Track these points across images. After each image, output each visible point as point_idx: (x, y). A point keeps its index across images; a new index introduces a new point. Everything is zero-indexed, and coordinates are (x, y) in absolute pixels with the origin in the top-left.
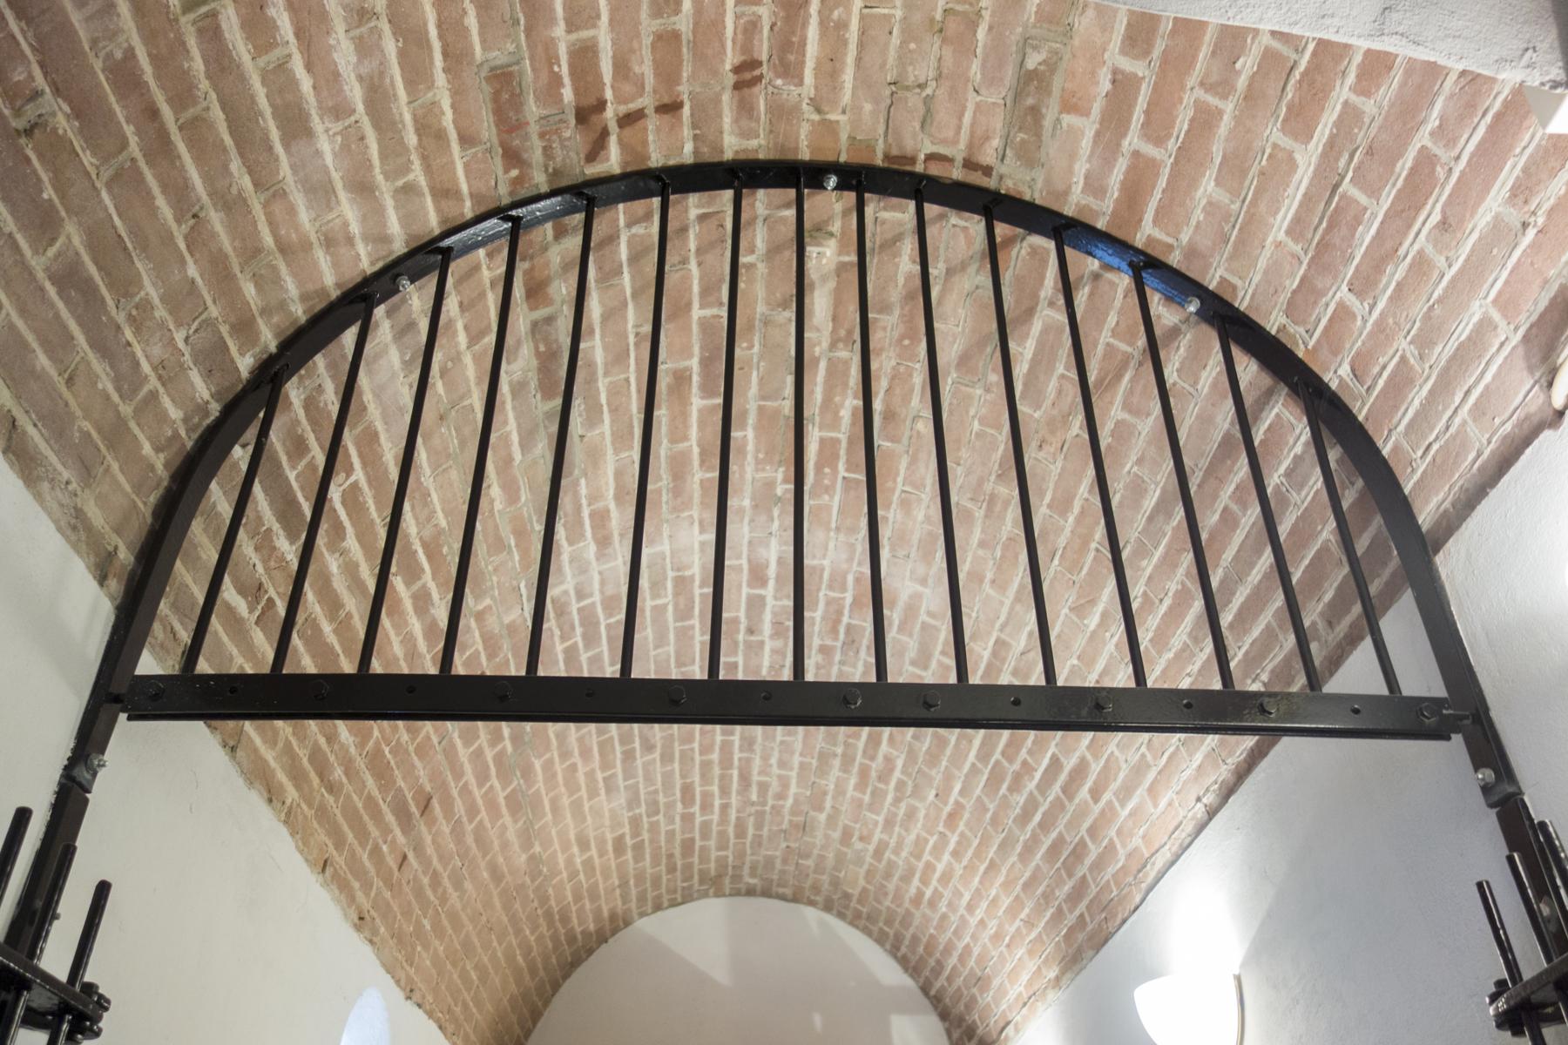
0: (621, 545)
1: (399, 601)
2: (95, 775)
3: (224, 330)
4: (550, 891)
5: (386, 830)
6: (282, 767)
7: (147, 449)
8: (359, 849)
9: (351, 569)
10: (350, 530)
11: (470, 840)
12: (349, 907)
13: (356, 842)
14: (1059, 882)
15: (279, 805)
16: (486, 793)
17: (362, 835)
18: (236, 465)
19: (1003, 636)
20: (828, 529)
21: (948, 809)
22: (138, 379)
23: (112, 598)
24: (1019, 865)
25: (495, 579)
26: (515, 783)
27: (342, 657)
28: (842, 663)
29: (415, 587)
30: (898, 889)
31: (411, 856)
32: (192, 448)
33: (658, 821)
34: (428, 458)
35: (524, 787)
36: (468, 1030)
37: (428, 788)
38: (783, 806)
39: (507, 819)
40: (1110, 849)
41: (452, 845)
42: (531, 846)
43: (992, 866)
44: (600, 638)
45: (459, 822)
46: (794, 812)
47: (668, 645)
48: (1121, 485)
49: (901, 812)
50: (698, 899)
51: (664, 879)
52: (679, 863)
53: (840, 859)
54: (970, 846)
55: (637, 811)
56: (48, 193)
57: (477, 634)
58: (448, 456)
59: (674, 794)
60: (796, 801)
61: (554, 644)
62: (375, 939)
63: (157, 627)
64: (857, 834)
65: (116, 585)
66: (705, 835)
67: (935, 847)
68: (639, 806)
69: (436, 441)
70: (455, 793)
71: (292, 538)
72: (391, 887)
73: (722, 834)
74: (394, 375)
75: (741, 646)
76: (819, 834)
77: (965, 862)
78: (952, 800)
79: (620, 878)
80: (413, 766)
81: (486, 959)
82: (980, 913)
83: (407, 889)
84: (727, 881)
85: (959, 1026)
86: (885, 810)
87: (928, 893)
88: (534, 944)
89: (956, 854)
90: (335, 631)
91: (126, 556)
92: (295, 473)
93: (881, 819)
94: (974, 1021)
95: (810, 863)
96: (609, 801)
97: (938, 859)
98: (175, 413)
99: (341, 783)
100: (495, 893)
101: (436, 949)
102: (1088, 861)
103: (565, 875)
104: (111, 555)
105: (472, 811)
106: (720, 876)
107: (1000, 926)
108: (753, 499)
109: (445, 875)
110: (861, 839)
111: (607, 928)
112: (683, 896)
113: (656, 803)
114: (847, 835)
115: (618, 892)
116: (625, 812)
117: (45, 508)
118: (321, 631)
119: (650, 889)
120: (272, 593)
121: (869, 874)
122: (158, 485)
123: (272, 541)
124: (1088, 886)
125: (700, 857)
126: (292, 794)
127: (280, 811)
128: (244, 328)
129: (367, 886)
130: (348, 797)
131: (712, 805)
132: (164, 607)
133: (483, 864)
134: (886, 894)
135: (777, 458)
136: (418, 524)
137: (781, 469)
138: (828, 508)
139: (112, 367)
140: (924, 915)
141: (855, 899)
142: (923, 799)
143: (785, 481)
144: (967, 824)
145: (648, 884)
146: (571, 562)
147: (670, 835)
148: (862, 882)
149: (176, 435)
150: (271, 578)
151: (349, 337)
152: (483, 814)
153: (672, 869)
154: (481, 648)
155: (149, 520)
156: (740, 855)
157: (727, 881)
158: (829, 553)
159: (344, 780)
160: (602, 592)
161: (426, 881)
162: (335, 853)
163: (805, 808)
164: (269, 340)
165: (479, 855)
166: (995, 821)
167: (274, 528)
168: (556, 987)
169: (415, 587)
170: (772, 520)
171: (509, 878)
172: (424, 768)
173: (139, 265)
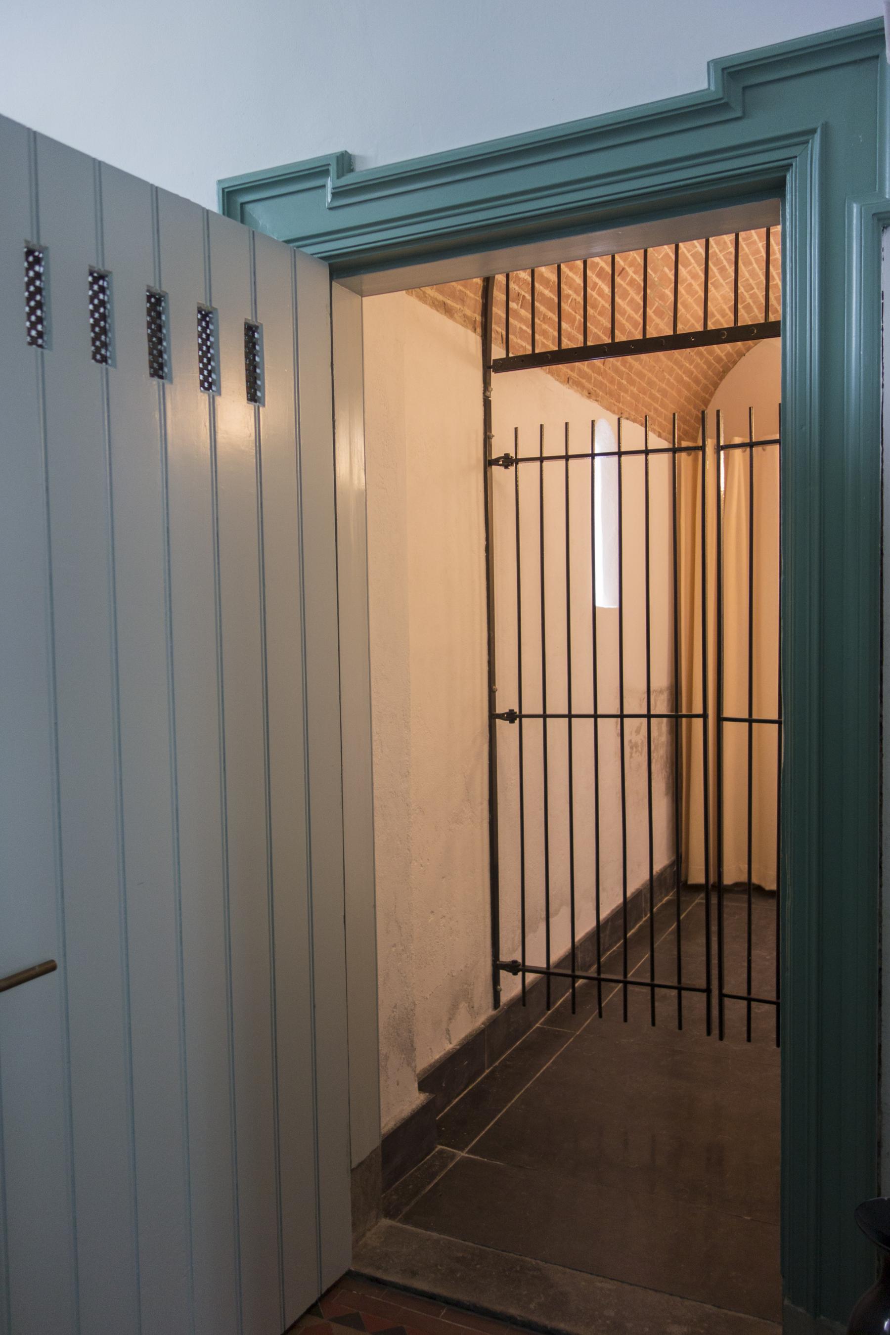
12: (583, 391)
18: (500, 282)
23: (478, 335)
26: (657, 304)
35: (662, 304)
36: (660, 420)
62: (598, 399)
63: (493, 335)
65: (479, 330)
80: (599, 321)
88: (694, 369)
91: (479, 318)
120: (523, 293)
132: (493, 326)
168: (716, 385)
172: (605, 319)
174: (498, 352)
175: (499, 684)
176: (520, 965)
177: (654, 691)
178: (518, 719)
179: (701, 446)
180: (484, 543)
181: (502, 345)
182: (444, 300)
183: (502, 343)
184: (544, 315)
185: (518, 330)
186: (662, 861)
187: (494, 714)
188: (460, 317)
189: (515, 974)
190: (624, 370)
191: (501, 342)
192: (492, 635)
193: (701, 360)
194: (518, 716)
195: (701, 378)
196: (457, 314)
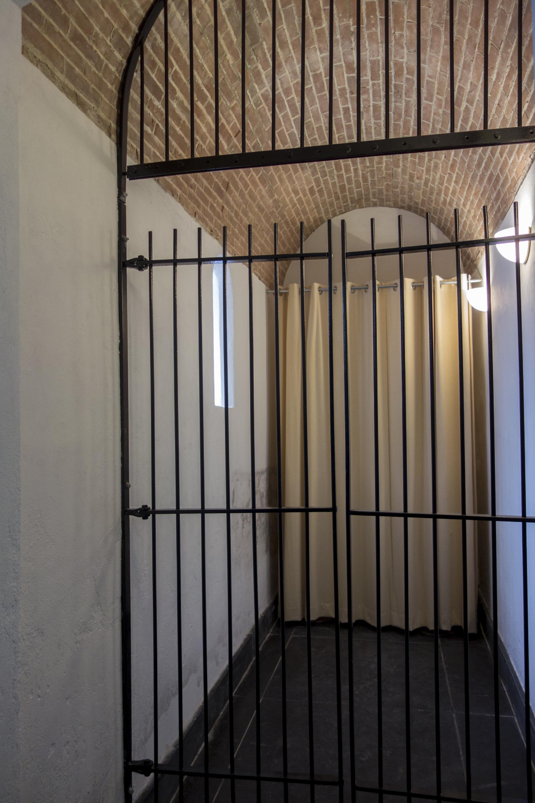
0: (286, 66)
1: (201, 111)
2: (125, 198)
3: (120, 31)
4: (285, 212)
5: (214, 198)
6: (174, 183)
7: (109, 85)
8: (206, 207)
9: (181, 104)
10: (177, 89)
11: (247, 197)
13: (204, 204)
14: (492, 193)
15: (176, 196)
16: (250, 178)
17: (206, 202)
19: (461, 85)
20: (378, 43)
21: (451, 162)
22: (101, 61)
23: (114, 141)
24: (479, 186)
25: (236, 92)
27: (185, 138)
28: (395, 102)
29: (206, 104)
30: (436, 199)
31: (225, 206)
32: (122, 79)
33: (327, 179)
34: (200, 52)
35: (265, 173)
37: (227, 180)
38: (381, 167)
39: (261, 187)
40: (506, 178)
41: (241, 200)
42: (274, 196)
43: (470, 187)
44: (285, 106)
45: (241, 190)
46: (387, 169)
47: (316, 104)
48: (497, 15)
49: (432, 165)
50: (352, 210)
51: (335, 203)
52: (340, 196)
53: (411, 188)
54: (461, 178)
55: (317, 176)
56: (64, 11)
57: (233, 116)
58: (207, 48)
59: (332, 167)
60: (387, 164)
61: (266, 113)
63: (128, 148)
64: (416, 176)
65: (114, 136)
66: (349, 183)
67: (448, 180)
68: (317, 174)
69: (201, 44)
70: (238, 180)
71: (159, 99)
72: (219, 218)
73: (357, 182)
74: (180, 23)
75: (349, 100)
76: (400, 178)
77: (460, 186)
78: (451, 159)
79: (315, 205)
81: (263, 242)
82: (468, 207)
83: (226, 219)
84: (363, 201)
85: (465, 255)
86: (426, 165)
87: (448, 200)
88: (282, 234)
89: (456, 182)
90: (181, 129)
91: (114, 126)
92: (154, 75)
93: (424, 169)
94: (469, 252)
95: (398, 190)
96: (303, 173)
97: (450, 185)
98: (113, 69)
99: (195, 184)
100: (262, 216)
101: (242, 240)
102: (500, 183)
103: (290, 206)
104: (110, 127)
105: (246, 186)
106: (360, 199)
107: (475, 212)
108: (341, 34)
109: (240, 212)
110: (418, 178)
111: (314, 225)
112: (345, 209)
113: (325, 171)
114: (411, 177)
115: (315, 210)
116: (311, 177)
117: (90, 118)
118: (176, 130)
119: (329, 208)
120: (157, 122)
121: (424, 193)
122: (115, 97)
123: (153, 103)
124: (501, 194)
125: (349, 192)
126: (179, 192)
127: (177, 198)
128: (126, 28)
129: (211, 219)
130: (198, 188)
131: (350, 170)
133: (254, 206)
134: (432, 201)
135: (348, 15)
136: (201, 78)
137: (351, 19)
138: (376, 33)
139: (93, 62)
140: (448, 209)
141: (420, 205)
142: (440, 159)
143: (353, 25)
144: (459, 169)
145: (328, 206)
146: (266, 77)
147: (334, 184)
148: (421, 197)
149: (116, 77)
150: (155, 116)
151: (161, 16)
152: (251, 186)
153: (337, 198)
154: (236, 121)
155: (116, 111)
156: (367, 189)
157: (363, 201)
158: (380, 53)
159: (196, 183)
160: (282, 87)
161: (233, 215)
162: (197, 209)
163: (392, 167)
164: (134, 27)
165: (252, 202)
166: (469, 167)
167: (153, 98)
169: (206, 104)
170: (352, 42)
171: (266, 210)
173: (91, 21)
174: (131, 161)
175: (132, 481)
176: (152, 765)
177: (258, 472)
178: (151, 515)
179: (327, 253)
180: (117, 341)
181: (137, 160)
182: (76, 91)
183: (137, 158)
184: (175, 150)
185: (152, 153)
186: (264, 605)
187: (127, 511)
188: (94, 116)
189: (147, 775)
190: (237, 221)
191: (136, 158)
192: (125, 432)
193: (287, 228)
194: (151, 512)
195: (287, 243)
196: (91, 112)
